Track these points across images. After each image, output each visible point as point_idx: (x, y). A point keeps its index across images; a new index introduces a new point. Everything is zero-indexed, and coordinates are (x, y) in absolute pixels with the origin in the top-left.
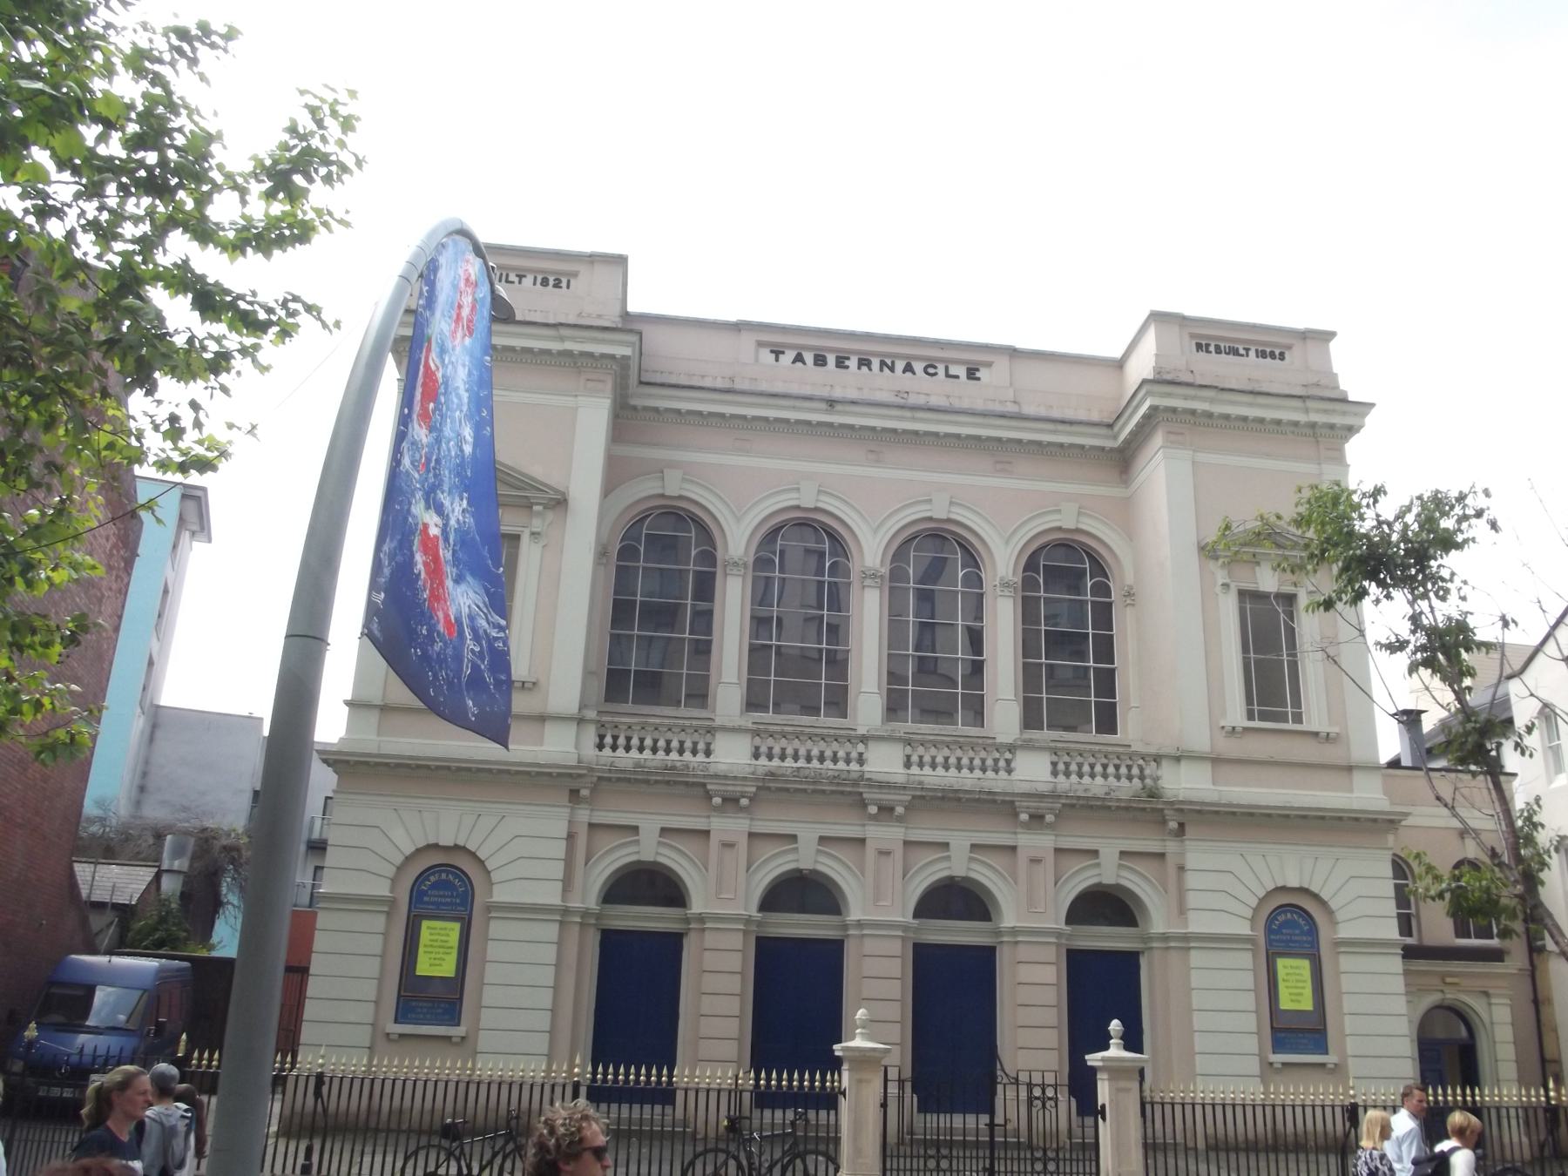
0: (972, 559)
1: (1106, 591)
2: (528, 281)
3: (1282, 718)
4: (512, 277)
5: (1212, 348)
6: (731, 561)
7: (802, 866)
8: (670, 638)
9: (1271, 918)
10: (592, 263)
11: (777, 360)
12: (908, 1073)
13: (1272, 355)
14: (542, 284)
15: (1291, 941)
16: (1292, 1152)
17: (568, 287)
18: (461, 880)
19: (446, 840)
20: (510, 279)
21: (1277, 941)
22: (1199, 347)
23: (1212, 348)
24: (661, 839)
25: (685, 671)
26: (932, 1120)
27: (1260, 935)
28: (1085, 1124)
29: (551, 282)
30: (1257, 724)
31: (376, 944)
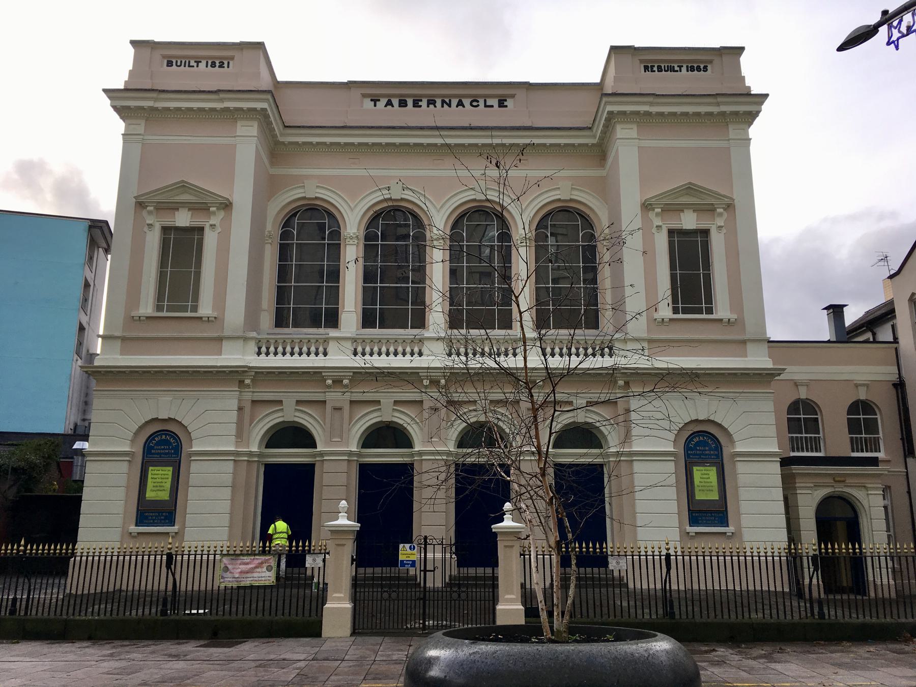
2: (202, 65)
3: (700, 311)
4: (192, 63)
5: (655, 69)
6: (349, 236)
8: (418, 287)
10: (242, 49)
11: (375, 105)
13: (699, 69)
14: (211, 66)
15: (703, 454)
17: (228, 67)
18: (174, 439)
19: (163, 415)
20: (191, 64)
21: (692, 454)
22: (646, 68)
23: (655, 69)
25: (324, 306)
27: (138, 449)
28: (601, 572)
29: (217, 64)
30: (165, 314)
31: (123, 479)
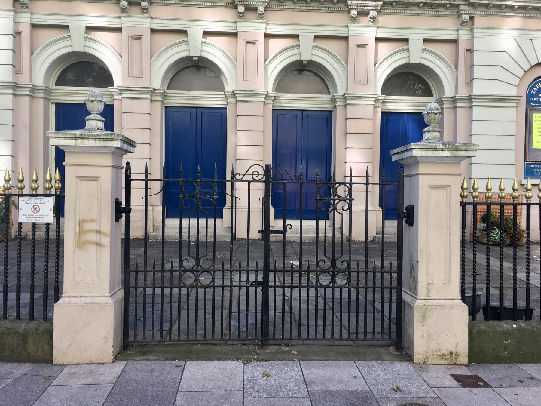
7: (192, 54)
9: (532, 85)
12: (157, 172)
16: (172, 243)
24: (204, 40)
26: (173, 223)
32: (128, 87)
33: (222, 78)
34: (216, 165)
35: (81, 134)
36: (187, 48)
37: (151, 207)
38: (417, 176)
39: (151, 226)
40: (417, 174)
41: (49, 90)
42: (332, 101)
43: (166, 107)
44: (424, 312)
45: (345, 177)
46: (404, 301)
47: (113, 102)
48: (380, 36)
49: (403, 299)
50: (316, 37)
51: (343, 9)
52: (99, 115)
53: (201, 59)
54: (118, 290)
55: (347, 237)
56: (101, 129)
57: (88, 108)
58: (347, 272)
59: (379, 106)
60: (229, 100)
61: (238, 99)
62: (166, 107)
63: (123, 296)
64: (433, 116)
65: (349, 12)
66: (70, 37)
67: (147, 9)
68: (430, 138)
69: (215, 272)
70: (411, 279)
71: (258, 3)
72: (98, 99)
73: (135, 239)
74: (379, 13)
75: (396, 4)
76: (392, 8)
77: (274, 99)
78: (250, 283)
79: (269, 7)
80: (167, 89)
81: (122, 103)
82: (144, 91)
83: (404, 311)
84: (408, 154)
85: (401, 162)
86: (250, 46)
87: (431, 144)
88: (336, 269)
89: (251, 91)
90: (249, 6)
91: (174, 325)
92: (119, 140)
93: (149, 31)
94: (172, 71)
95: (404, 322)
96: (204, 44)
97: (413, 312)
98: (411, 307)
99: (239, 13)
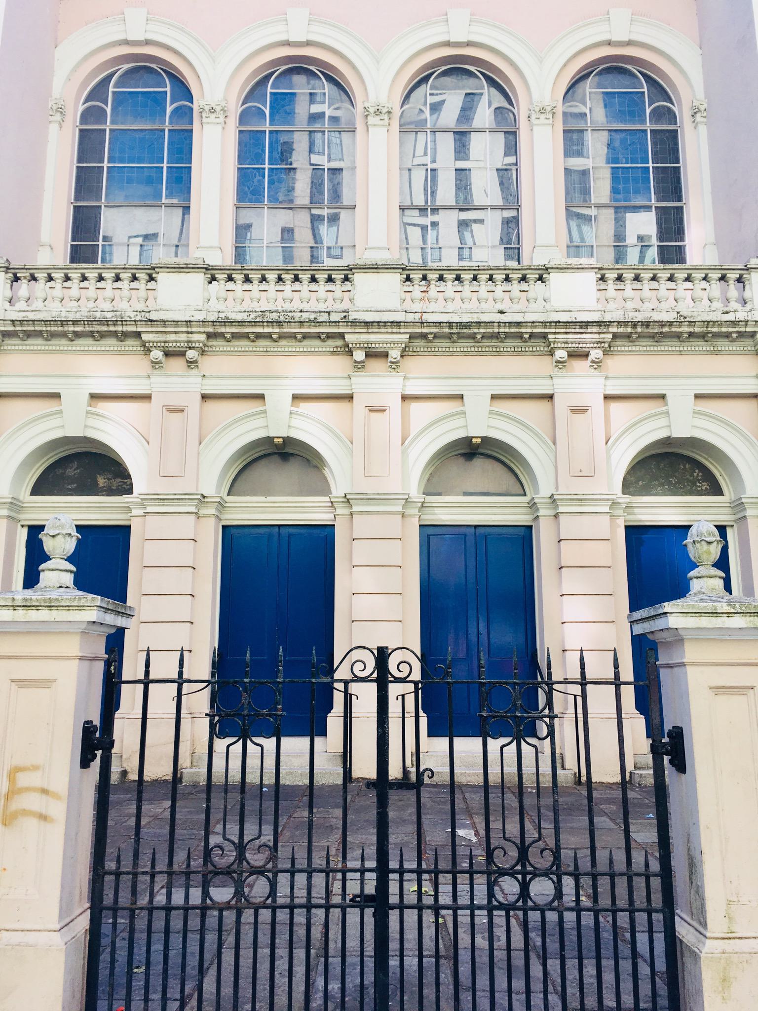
0: (183, 90)
1: (671, 116)
24: (293, 409)
32: (158, 494)
33: (326, 472)
34: (281, 650)
35: (25, 600)
36: (265, 424)
37: (190, 716)
38: (683, 667)
39: (188, 753)
40: (683, 665)
41: (18, 503)
42: (530, 507)
43: (224, 527)
44: (725, 969)
45: (563, 651)
46: (681, 941)
47: (130, 520)
48: (610, 391)
49: (677, 934)
50: (494, 397)
51: (542, 349)
52: (66, 560)
53: (288, 441)
54: (81, 914)
55: (575, 773)
56: (67, 587)
57: (45, 548)
58: (553, 874)
59: (620, 516)
60: (339, 511)
61: (355, 509)
62: (224, 527)
63: (88, 927)
64: (705, 546)
65: (551, 353)
66: (61, 412)
67: (196, 362)
68: (703, 590)
69: (275, 875)
70: (693, 892)
71: (389, 345)
72: (64, 532)
73: (156, 782)
74: (606, 353)
75: (637, 338)
76: (630, 344)
77: (422, 506)
78: (348, 898)
79: (409, 351)
80: (228, 495)
81: (145, 522)
82: (185, 499)
83: (683, 964)
84: (659, 624)
85: (650, 637)
86: (375, 416)
87: (705, 604)
88: (529, 868)
89: (378, 494)
90: (374, 350)
91: (193, 990)
92: (95, 608)
93: (199, 397)
94: (235, 466)
95: (684, 988)
96: (293, 416)
97: (700, 968)
98: (696, 957)
99: (356, 362)
